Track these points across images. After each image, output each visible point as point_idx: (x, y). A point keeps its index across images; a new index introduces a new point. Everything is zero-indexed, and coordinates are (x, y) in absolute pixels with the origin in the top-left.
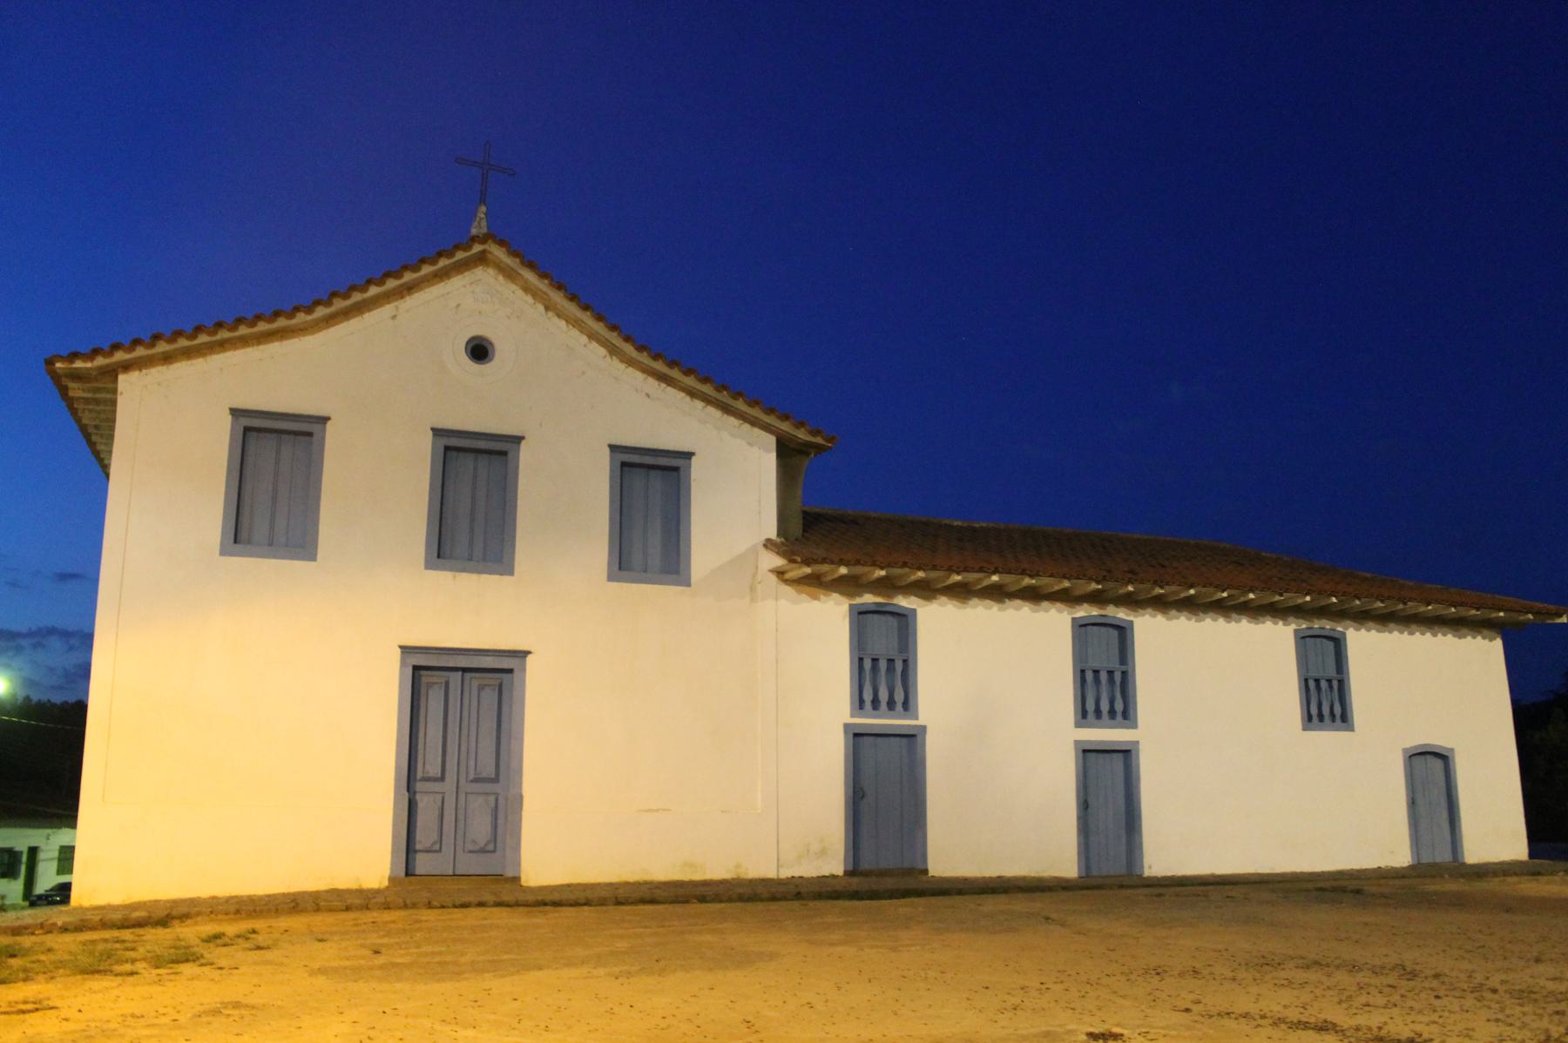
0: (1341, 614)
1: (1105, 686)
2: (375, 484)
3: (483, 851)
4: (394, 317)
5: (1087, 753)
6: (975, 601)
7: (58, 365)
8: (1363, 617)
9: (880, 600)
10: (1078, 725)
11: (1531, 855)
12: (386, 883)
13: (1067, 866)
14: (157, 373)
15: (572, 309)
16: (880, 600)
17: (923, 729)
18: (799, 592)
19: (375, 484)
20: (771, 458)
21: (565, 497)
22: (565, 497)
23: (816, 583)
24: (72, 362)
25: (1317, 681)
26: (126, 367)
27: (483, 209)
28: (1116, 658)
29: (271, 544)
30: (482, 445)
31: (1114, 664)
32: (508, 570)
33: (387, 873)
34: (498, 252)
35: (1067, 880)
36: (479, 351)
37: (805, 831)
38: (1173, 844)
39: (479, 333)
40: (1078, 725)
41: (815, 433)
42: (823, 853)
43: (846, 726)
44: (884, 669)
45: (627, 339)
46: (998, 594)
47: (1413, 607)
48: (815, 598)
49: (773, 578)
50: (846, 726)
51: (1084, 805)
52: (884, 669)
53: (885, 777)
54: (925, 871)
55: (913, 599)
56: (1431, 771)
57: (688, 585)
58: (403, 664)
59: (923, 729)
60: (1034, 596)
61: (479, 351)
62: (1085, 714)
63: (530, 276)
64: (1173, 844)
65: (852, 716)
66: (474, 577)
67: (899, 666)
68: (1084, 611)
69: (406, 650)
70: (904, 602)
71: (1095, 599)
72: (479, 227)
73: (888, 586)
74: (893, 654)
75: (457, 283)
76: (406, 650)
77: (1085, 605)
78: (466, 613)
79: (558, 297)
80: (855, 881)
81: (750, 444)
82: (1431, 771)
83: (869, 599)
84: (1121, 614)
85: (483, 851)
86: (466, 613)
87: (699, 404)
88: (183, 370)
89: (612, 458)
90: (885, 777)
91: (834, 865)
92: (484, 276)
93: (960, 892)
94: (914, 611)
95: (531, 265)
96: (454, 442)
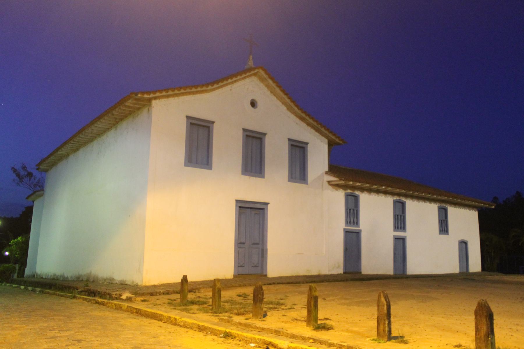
0: (406, 196)
1: (400, 221)
2: (227, 146)
3: (255, 266)
4: (231, 90)
5: (396, 239)
6: (372, 193)
7: (139, 95)
8: (412, 197)
9: (351, 192)
10: (394, 231)
11: (483, 268)
12: (232, 277)
13: (391, 272)
14: (164, 101)
15: (281, 94)
16: (351, 192)
17: (361, 230)
18: (333, 188)
19: (227, 146)
20: (326, 146)
21: (276, 153)
22: (276, 153)
23: (338, 186)
24: (143, 95)
25: (398, 216)
26: (155, 98)
27: (251, 57)
28: (401, 212)
29: (197, 163)
30: (297, 144)
31: (444, 219)
32: (263, 177)
33: (233, 274)
34: (262, 73)
35: (390, 275)
36: (253, 104)
37: (332, 262)
38: (415, 266)
39: (253, 98)
40: (394, 231)
41: (341, 140)
42: (338, 267)
43: (344, 229)
44: (352, 213)
45: (297, 106)
46: (378, 192)
47: (467, 202)
48: (337, 190)
49: (327, 183)
50: (344, 229)
51: (395, 254)
52: (352, 213)
53: (352, 243)
54: (361, 273)
55: (359, 192)
56: (464, 245)
57: (307, 184)
58: (236, 206)
59: (361, 230)
60: (386, 193)
61: (253, 104)
62: (348, 222)
63: (270, 81)
64: (415, 266)
65: (345, 226)
66: (254, 178)
67: (355, 211)
68: (396, 198)
69: (237, 201)
70: (357, 193)
71: (399, 195)
72: (251, 63)
73: (354, 188)
74: (401, 214)
75: (247, 80)
76: (237, 201)
77: (396, 196)
78: (253, 190)
79: (278, 90)
80: (348, 276)
81: (322, 141)
82: (464, 245)
83: (349, 191)
84: (403, 199)
85: (255, 266)
86: (253, 190)
87: (309, 128)
88: (173, 101)
89: (187, 122)
90: (352, 243)
91: (340, 271)
92: (255, 79)
93: (381, 279)
94: (359, 195)
95: (272, 79)
96: (193, 122)
